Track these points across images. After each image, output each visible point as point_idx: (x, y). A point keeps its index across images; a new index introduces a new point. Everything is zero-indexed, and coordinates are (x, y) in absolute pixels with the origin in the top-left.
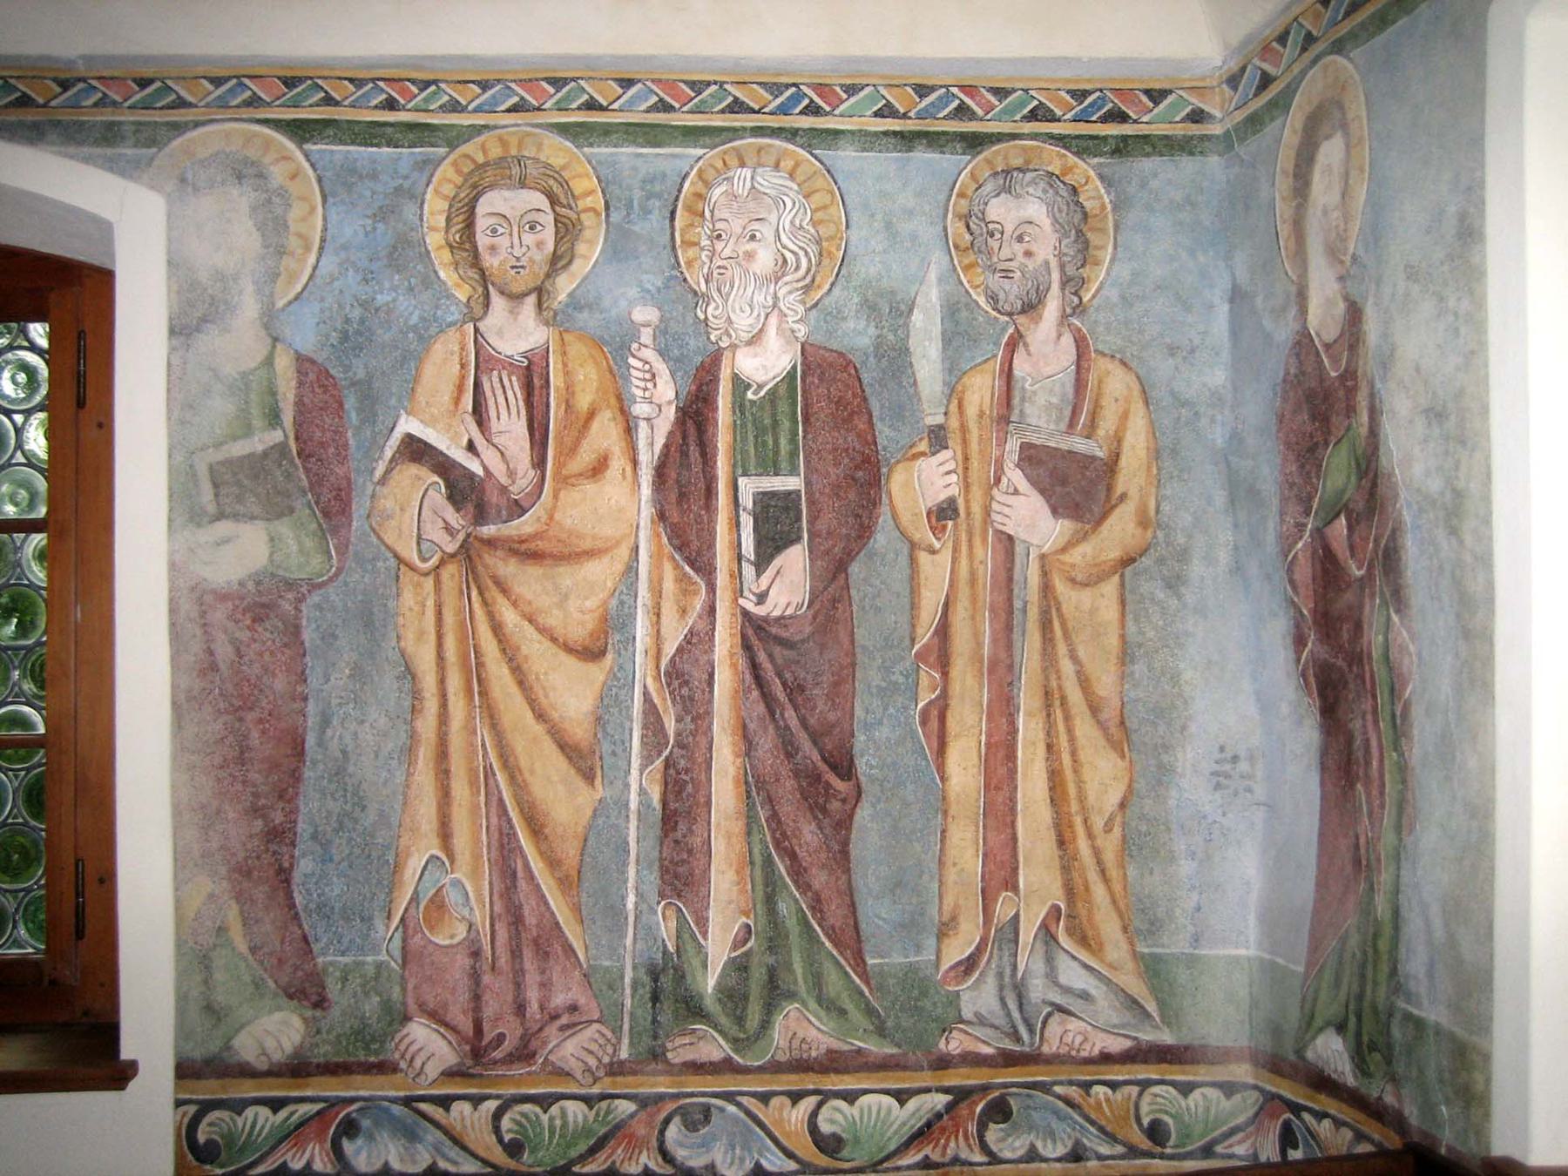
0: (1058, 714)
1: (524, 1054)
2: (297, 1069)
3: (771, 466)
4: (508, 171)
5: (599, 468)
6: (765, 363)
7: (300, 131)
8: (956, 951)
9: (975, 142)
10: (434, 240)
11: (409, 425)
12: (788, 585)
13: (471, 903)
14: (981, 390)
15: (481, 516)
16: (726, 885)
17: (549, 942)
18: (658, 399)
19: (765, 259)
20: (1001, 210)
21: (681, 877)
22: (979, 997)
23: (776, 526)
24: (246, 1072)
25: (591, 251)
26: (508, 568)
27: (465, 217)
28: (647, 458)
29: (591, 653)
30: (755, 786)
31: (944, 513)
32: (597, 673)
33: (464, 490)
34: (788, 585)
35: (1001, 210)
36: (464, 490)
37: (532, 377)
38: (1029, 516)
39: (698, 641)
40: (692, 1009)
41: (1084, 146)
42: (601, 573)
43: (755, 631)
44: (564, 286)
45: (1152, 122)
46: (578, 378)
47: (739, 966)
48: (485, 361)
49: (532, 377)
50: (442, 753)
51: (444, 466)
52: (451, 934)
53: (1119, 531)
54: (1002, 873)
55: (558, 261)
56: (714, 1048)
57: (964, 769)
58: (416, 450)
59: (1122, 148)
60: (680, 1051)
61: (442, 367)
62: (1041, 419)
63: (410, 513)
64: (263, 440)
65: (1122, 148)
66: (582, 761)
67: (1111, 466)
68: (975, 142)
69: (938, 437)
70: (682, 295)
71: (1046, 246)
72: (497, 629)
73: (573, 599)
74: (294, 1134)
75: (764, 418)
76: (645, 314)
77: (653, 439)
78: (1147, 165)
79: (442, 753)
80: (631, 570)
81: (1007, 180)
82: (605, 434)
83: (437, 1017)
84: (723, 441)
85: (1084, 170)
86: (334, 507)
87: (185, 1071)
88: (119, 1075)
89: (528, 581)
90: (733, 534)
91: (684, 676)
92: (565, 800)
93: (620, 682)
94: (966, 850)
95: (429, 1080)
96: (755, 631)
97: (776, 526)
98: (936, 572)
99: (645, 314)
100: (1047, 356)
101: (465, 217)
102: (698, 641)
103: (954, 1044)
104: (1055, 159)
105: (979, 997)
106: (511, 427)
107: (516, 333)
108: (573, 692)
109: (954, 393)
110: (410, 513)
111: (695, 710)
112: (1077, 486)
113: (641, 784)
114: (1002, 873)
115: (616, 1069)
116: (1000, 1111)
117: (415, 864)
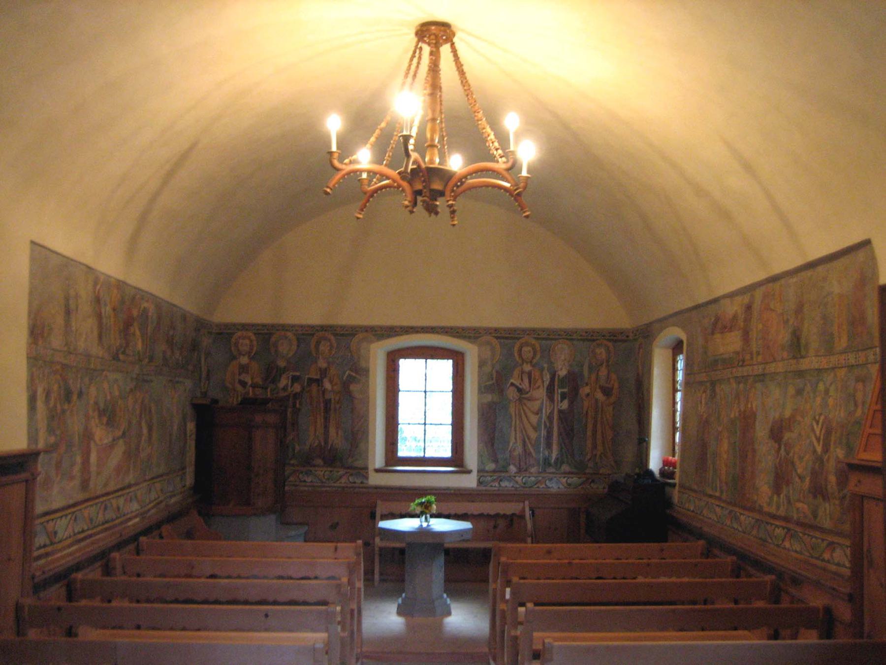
0: (415, 60)
1: (526, 470)
2: (494, 471)
3: (563, 387)
4: (527, 344)
5: (539, 387)
6: (563, 373)
7: (497, 338)
8: (588, 457)
9: (594, 340)
10: (516, 355)
11: (512, 381)
12: (565, 405)
13: (519, 450)
14: (593, 377)
15: (521, 394)
16: (555, 447)
17: (530, 454)
18: (547, 378)
19: (563, 358)
20: (598, 351)
21: (549, 445)
22: (590, 464)
23: (563, 396)
24: (487, 472)
25: (538, 356)
26: (525, 401)
27: (520, 350)
28: (545, 386)
29: (537, 414)
30: (560, 434)
31: (588, 395)
32: (537, 417)
33: (520, 390)
34: (565, 405)
35: (598, 351)
36: (520, 390)
37: (530, 374)
38: (599, 396)
39: (552, 413)
40: (550, 465)
41: (610, 340)
42: (539, 402)
43: (560, 412)
44: (535, 361)
45: (620, 337)
46: (536, 374)
47: (557, 459)
48: (523, 372)
49: (530, 374)
50: (515, 428)
51: (517, 387)
52: (516, 453)
53: (613, 399)
54: (595, 447)
55: (533, 358)
56: (553, 470)
57: (589, 433)
58: (512, 384)
59: (616, 341)
60: (548, 471)
61: (516, 373)
62: (602, 382)
63: (512, 393)
64: (491, 383)
65: (616, 341)
66: (536, 429)
67: (612, 388)
68: (594, 340)
69: (587, 384)
70: (551, 363)
71: (604, 356)
72: (524, 411)
73: (536, 405)
74: (493, 481)
75: (563, 382)
76: (546, 365)
77: (547, 383)
78: (619, 343)
79: (515, 428)
80: (542, 403)
81: (598, 345)
82: (539, 383)
83: (515, 465)
84: (556, 383)
85: (610, 344)
86: (502, 392)
87: (478, 472)
88: (103, 575)
89: (529, 404)
90: (557, 397)
91: (550, 418)
92: (533, 435)
93: (541, 418)
94: (589, 443)
95: (513, 474)
96: (560, 412)
97: (563, 396)
98: (586, 403)
99: (546, 365)
100: (603, 372)
101: (520, 350)
102: (552, 413)
103: (587, 471)
104: (605, 342)
105: (590, 464)
106: (526, 381)
107: (527, 368)
108: (534, 419)
109: (589, 378)
110: (512, 393)
111: (551, 422)
112: (607, 392)
113: (543, 433)
114: (595, 447)
115: (539, 473)
116: (593, 481)
117: (511, 444)
